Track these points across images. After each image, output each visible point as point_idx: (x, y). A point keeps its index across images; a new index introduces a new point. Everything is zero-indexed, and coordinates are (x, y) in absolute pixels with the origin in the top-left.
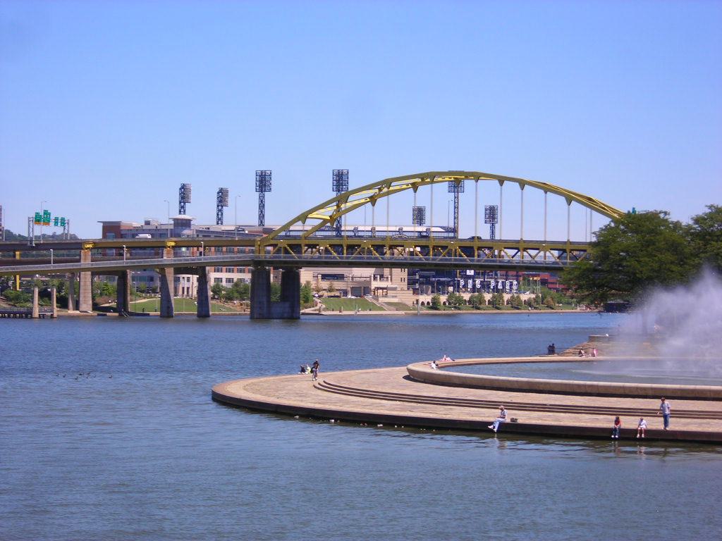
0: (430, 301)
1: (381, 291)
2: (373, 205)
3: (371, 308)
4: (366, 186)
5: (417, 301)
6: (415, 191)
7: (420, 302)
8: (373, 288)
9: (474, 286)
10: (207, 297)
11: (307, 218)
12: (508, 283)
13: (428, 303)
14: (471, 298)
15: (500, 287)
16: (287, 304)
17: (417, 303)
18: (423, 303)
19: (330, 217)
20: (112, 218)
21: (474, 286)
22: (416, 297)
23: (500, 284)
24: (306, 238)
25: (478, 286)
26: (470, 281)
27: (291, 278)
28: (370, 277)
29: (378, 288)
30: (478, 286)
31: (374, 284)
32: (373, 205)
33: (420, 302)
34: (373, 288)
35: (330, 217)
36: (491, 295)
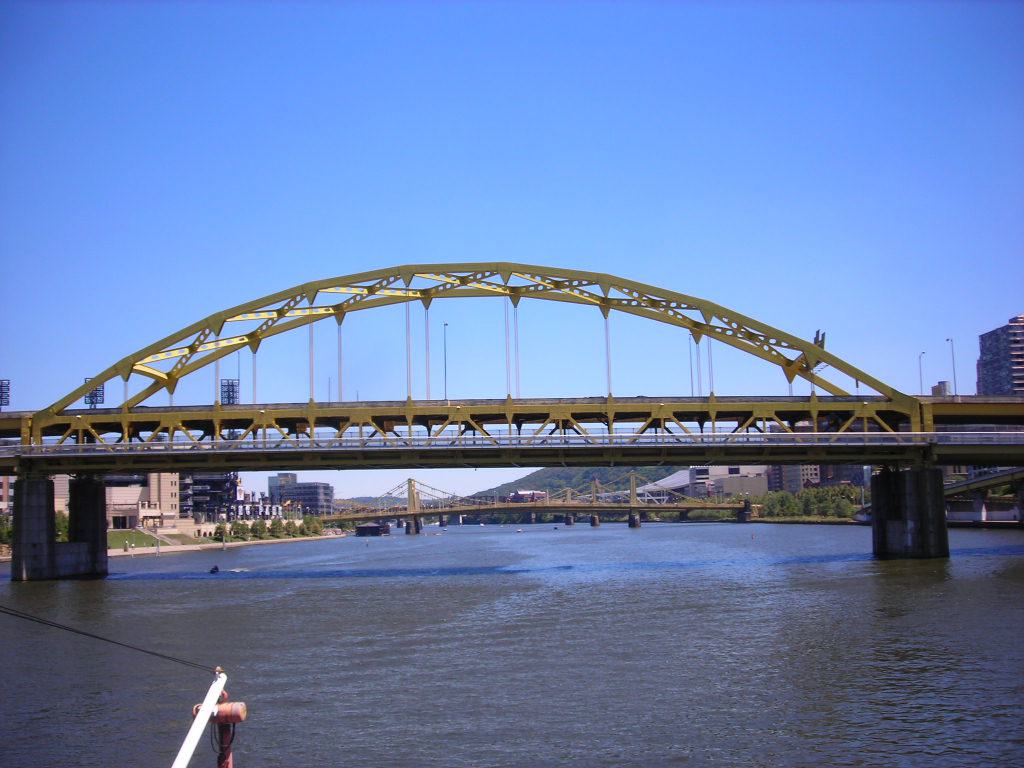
0: (213, 533)
1: (151, 521)
2: (255, 350)
3: (153, 542)
4: (239, 307)
5: (199, 531)
6: (340, 322)
7: (202, 533)
8: (141, 517)
9: (244, 511)
10: (995, 466)
11: (132, 370)
12: (274, 508)
13: (210, 533)
14: (254, 525)
15: (267, 513)
16: (84, 547)
17: (199, 535)
18: (205, 534)
19: (168, 374)
20: (216, 701)
21: (244, 511)
22: (198, 527)
23: (267, 510)
24: (131, 409)
25: (248, 513)
26: (241, 507)
27: (88, 498)
28: (137, 504)
29: (145, 517)
30: (248, 513)
31: (143, 513)
32: (255, 350)
33: (202, 533)
34: (141, 517)
35: (168, 374)
36: (301, 521)
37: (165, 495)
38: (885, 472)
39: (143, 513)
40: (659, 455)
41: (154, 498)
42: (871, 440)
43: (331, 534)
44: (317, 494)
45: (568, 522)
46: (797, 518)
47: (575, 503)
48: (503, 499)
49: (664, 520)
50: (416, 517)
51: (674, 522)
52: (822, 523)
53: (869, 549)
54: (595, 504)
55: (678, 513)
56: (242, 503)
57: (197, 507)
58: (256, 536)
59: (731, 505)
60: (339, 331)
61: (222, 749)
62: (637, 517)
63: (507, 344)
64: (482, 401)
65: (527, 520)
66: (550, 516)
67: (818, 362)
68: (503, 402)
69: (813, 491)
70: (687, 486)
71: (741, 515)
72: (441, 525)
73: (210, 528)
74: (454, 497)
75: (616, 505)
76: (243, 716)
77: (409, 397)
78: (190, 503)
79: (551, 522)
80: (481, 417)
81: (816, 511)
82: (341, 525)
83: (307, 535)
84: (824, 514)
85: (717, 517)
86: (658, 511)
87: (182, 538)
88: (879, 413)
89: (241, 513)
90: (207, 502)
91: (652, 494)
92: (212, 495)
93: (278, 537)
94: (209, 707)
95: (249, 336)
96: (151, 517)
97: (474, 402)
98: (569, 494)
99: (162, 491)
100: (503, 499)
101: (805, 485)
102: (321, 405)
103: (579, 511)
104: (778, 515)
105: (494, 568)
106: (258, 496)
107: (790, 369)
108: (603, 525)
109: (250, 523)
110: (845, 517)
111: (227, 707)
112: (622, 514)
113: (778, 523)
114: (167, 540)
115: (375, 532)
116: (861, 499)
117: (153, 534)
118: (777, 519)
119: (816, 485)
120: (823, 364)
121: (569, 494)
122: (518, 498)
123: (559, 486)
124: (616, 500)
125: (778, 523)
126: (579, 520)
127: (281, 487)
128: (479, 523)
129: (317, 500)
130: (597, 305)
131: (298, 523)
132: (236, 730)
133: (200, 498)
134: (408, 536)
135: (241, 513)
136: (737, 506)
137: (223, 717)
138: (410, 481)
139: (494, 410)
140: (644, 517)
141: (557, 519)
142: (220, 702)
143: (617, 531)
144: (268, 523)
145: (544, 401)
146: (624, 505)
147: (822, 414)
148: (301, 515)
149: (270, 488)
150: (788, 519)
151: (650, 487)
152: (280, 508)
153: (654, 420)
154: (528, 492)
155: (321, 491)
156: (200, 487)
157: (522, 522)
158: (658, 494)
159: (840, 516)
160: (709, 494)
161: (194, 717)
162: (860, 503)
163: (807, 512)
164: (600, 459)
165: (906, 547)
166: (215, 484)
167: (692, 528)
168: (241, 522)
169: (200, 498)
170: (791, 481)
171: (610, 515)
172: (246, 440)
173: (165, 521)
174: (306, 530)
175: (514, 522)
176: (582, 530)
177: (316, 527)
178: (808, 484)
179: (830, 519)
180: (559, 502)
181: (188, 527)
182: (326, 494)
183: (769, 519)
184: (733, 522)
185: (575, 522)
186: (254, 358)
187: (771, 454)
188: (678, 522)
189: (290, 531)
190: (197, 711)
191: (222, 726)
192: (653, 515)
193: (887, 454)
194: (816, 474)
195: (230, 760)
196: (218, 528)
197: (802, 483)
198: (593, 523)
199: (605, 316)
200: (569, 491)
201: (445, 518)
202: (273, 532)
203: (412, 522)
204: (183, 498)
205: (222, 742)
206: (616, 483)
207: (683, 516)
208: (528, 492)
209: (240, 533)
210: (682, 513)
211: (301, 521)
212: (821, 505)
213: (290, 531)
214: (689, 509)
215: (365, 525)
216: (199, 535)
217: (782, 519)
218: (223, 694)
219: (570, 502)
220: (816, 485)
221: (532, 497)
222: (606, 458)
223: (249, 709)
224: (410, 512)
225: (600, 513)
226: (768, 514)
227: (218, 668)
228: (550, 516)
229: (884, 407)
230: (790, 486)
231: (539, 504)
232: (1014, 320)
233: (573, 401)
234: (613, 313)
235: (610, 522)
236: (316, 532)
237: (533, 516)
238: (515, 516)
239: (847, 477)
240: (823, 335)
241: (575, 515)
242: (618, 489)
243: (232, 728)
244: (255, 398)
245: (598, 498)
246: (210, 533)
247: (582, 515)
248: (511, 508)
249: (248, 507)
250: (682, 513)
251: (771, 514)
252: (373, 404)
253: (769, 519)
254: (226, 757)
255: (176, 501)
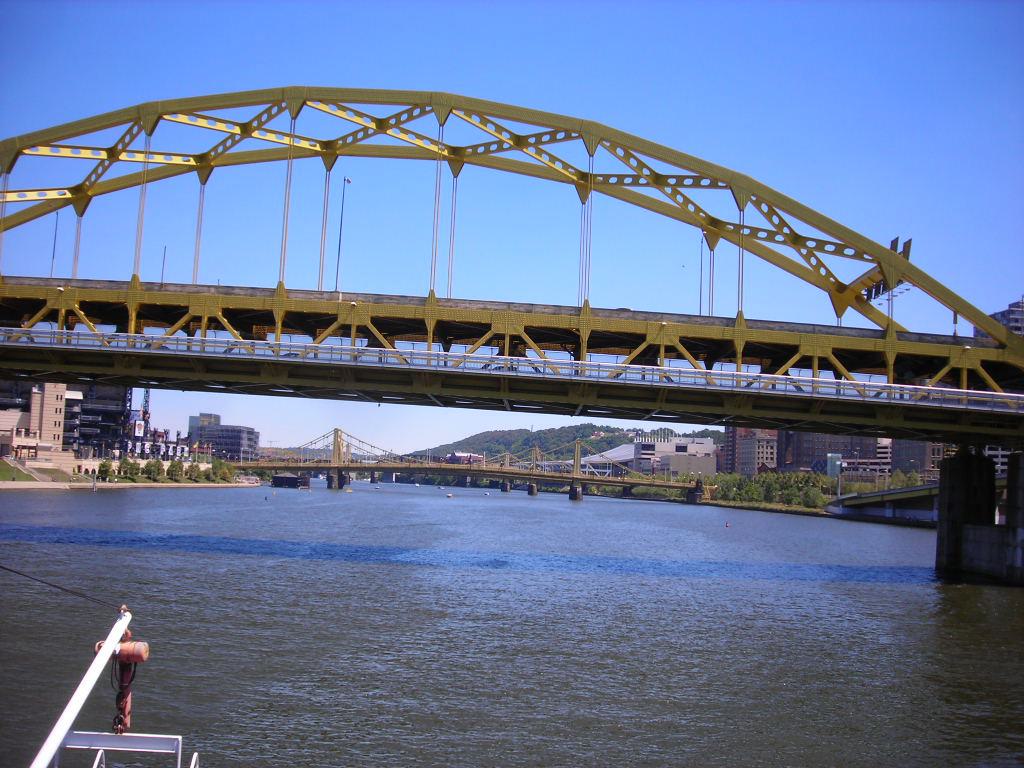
2: (81, 213)
5: (79, 467)
6: (204, 181)
7: (90, 471)
9: (143, 451)
13: (94, 471)
14: (148, 465)
17: (79, 471)
21: (143, 451)
22: (79, 462)
23: (171, 449)
25: (147, 451)
26: (139, 444)
28: (12, 430)
30: (147, 451)
33: (83, 470)
37: (48, 425)
38: (963, 455)
39: (17, 441)
40: (654, 400)
41: (34, 425)
42: (970, 402)
43: (245, 482)
44: (240, 438)
45: (504, 489)
46: (756, 505)
47: (515, 469)
48: (436, 459)
49: (605, 494)
50: (339, 470)
51: (616, 497)
52: (787, 512)
53: (930, 561)
54: (536, 471)
55: (621, 488)
56: (142, 440)
57: (86, 439)
58: (149, 478)
59: (681, 484)
60: (202, 192)
61: (121, 687)
62: (579, 489)
63: (436, 213)
64: (390, 297)
65: (461, 483)
66: (485, 481)
67: (900, 282)
68: (423, 301)
69: (772, 476)
70: (631, 461)
71: (691, 496)
72: (371, 482)
73: (92, 464)
74: (390, 454)
75: (558, 475)
76: (145, 656)
77: (280, 284)
78: (76, 434)
79: (486, 487)
80: (397, 326)
81: (778, 498)
82: (261, 473)
83: (213, 481)
84: (789, 502)
85: (665, 496)
86: (600, 484)
87: (56, 474)
88: (985, 364)
89: (138, 451)
90: (97, 435)
91: (595, 466)
92: (102, 428)
93: (177, 481)
94: (111, 645)
95: (72, 190)
96: (24, 447)
97: (379, 299)
98: (507, 461)
99: (44, 419)
100: (436, 459)
101: (759, 469)
102: (150, 286)
103: (517, 478)
104: (734, 499)
105: (384, 550)
106: (173, 437)
107: (842, 296)
108: (541, 495)
109: (143, 463)
110: (815, 507)
111: (130, 646)
112: (562, 484)
113: (734, 507)
114: (35, 475)
115: (292, 483)
116: (836, 488)
117: (20, 467)
118: (732, 503)
119: (773, 470)
120: (906, 285)
121: (507, 461)
122: (454, 460)
123: (498, 452)
124: (557, 468)
125: (734, 507)
126: (516, 487)
127: (202, 428)
128: (413, 482)
129: (239, 445)
130: (572, 182)
131: (204, 467)
132: (137, 673)
133: (88, 430)
134: (329, 491)
135: (138, 451)
136: (687, 485)
137: (124, 656)
138: (336, 431)
139: (408, 313)
140: (586, 491)
141: (493, 485)
142: (122, 640)
143: (556, 503)
144: (166, 465)
145: (485, 305)
146: (565, 475)
147: (901, 359)
148: (210, 459)
149: (191, 427)
150: (745, 504)
151: (596, 458)
152: (187, 449)
153: (651, 347)
154: (465, 455)
155: (245, 435)
156: (90, 418)
157: (457, 485)
158: (604, 466)
159: (808, 507)
160: (653, 471)
161: (96, 654)
162: (836, 494)
163: (768, 498)
164: (563, 400)
165: (1012, 567)
166: (107, 415)
167: (636, 506)
168: (131, 461)
169: (88, 430)
170: (745, 464)
171: (550, 485)
172: (42, 333)
173: (39, 452)
174: (212, 475)
175: (447, 484)
176: (517, 500)
177: (225, 473)
178: (763, 468)
179: (794, 508)
180: (496, 467)
181: (67, 462)
182: (249, 439)
183: (723, 503)
184: (682, 502)
185: (511, 488)
186: (79, 222)
187: (823, 412)
188: (620, 497)
189: (193, 475)
190: (100, 647)
191: (123, 665)
192: (594, 488)
193: (991, 426)
194: (772, 459)
195: (129, 699)
196: (102, 466)
197: (757, 466)
198: (531, 491)
199: (583, 199)
200: (508, 456)
201: (377, 474)
202: (172, 475)
203: (335, 477)
204: (68, 429)
205: (122, 680)
206: (556, 453)
207: (627, 492)
208: (465, 455)
209: (129, 473)
210: (625, 488)
211: (210, 466)
212: (786, 492)
213: (193, 475)
214: (634, 485)
215: (282, 475)
216: (79, 471)
217: (738, 504)
218: (126, 633)
219: (507, 468)
220: (773, 470)
221: (469, 460)
222: (572, 399)
223: (152, 650)
224: (334, 464)
225: (538, 482)
226: (722, 498)
227: (124, 606)
228: (485, 481)
229: (993, 355)
230: (742, 469)
231: (475, 466)
232: (1016, 305)
233: (530, 308)
234: (595, 197)
235: (547, 491)
236: (224, 479)
237: (469, 479)
238: (450, 478)
239: (807, 464)
240: (908, 245)
241: (512, 482)
242: (558, 458)
243: (133, 669)
244: (74, 274)
245: (537, 466)
246: (94, 471)
247: (518, 482)
248: (444, 469)
249: (148, 445)
250: (625, 488)
251: (725, 497)
252: (228, 291)
253: (723, 503)
254: (125, 696)
255: (60, 431)
